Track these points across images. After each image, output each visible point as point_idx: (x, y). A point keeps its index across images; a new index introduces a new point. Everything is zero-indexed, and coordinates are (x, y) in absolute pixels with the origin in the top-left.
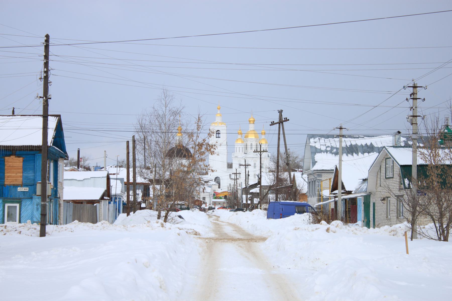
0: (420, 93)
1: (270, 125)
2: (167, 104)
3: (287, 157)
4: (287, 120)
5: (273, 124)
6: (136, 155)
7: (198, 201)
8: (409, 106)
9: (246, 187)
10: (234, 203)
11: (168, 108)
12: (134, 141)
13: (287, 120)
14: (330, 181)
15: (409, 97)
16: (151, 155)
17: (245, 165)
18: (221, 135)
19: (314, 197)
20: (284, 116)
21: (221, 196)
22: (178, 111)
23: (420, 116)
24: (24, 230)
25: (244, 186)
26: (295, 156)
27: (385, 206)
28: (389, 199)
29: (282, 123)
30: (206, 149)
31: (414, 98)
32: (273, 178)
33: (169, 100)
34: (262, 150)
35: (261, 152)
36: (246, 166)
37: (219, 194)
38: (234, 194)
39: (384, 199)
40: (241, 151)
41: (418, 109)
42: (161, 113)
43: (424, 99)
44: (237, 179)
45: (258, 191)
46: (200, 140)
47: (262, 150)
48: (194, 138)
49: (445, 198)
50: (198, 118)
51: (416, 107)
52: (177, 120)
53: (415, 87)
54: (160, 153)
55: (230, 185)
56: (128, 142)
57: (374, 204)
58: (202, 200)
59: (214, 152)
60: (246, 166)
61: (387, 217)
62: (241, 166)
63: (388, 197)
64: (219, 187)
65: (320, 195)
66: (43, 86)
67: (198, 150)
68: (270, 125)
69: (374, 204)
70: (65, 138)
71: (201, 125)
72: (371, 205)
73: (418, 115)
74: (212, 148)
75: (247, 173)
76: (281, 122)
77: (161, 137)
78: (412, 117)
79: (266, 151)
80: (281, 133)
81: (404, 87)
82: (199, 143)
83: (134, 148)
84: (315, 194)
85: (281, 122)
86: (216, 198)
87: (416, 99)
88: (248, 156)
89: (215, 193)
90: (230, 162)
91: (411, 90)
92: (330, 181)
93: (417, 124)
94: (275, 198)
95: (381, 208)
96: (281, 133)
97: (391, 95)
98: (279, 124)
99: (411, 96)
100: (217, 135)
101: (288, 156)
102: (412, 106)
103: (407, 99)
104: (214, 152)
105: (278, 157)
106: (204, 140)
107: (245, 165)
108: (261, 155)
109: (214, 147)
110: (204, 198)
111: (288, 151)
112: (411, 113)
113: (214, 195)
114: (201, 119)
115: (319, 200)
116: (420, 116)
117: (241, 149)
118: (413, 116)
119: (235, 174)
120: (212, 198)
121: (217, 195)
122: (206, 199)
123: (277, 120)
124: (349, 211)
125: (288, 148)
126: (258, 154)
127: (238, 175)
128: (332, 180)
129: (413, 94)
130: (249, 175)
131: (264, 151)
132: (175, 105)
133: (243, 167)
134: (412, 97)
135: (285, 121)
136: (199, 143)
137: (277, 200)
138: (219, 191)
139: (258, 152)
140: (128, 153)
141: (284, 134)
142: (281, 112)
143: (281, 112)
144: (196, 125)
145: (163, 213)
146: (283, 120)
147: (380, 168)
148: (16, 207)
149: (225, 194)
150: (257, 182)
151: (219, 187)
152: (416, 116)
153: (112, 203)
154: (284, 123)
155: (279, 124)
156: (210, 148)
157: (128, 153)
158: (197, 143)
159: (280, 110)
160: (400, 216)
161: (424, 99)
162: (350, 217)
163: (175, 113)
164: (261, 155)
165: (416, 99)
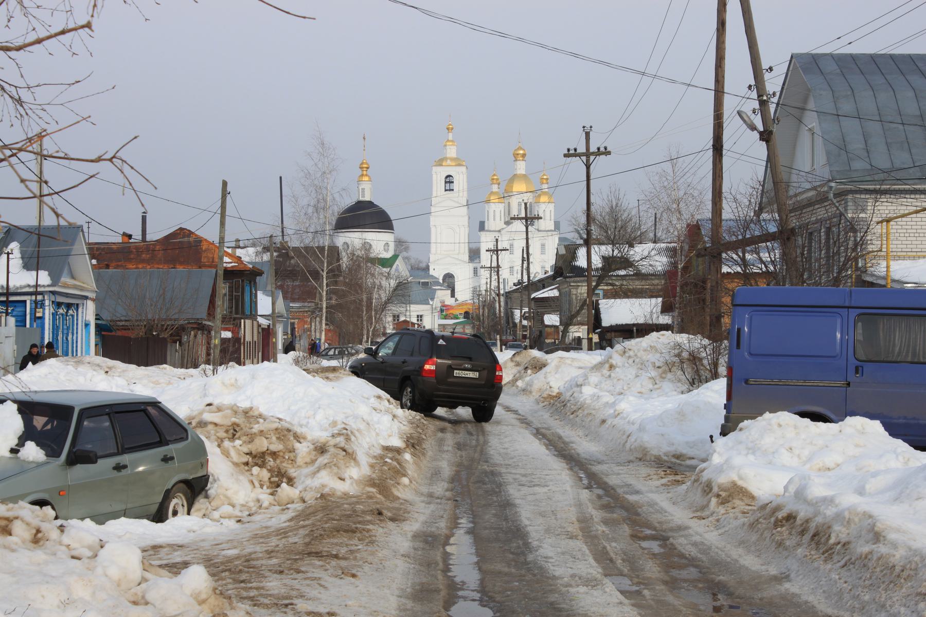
1: (565, 156)
18: (455, 186)
21: (457, 312)
24: (617, 359)
34: (593, 149)
45: (555, 293)
47: (593, 149)
58: (414, 320)
64: (453, 295)
68: (565, 156)
76: (588, 156)
77: (525, 475)
86: (446, 317)
90: (474, 246)
100: (448, 185)
108: (588, 167)
110: (420, 317)
113: (442, 311)
122: (424, 319)
125: (765, 66)
126: (578, 165)
131: (599, 153)
133: (519, 226)
138: (450, 301)
139: (580, 155)
148: (25, 302)
149: (465, 309)
151: (453, 295)
164: (588, 167)
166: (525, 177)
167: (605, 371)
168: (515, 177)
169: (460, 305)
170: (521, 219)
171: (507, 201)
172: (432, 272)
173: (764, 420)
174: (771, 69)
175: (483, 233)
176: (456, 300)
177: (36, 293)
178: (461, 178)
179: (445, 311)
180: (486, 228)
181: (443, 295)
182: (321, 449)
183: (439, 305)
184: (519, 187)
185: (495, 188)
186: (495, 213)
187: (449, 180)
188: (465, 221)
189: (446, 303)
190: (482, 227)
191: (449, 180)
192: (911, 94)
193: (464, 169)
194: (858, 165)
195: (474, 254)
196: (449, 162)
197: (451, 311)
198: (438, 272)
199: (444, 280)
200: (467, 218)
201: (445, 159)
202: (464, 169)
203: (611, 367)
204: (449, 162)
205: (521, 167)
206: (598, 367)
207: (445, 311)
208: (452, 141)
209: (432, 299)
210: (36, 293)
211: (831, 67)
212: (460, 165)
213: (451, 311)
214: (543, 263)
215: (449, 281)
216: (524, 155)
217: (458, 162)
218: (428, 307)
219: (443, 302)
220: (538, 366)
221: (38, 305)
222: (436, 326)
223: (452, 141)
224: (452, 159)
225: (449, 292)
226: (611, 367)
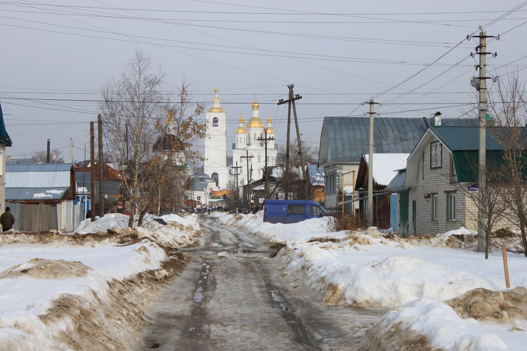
0: (490, 46)
1: (278, 104)
2: (142, 69)
3: (299, 144)
4: (299, 97)
5: (281, 102)
6: (104, 140)
7: (191, 200)
8: (474, 64)
9: (248, 184)
10: (236, 202)
11: (142, 76)
12: (100, 122)
13: (299, 97)
14: (354, 175)
15: (474, 51)
16: (119, 139)
17: (247, 157)
18: (219, 123)
19: (332, 195)
20: (295, 92)
21: (219, 195)
22: (156, 81)
23: (489, 78)
25: (246, 183)
26: (307, 146)
27: (430, 205)
28: (435, 196)
29: (293, 101)
30: (194, 129)
31: (482, 52)
32: (282, 172)
33: (144, 65)
34: (268, 138)
35: (266, 140)
36: (248, 158)
37: (216, 192)
38: (235, 192)
39: (428, 196)
40: (243, 142)
41: (487, 68)
42: (133, 82)
43: (496, 54)
44: (237, 174)
45: (263, 188)
46: (185, 118)
47: (268, 138)
48: (178, 116)
49: (493, 196)
50: (182, 90)
51: (485, 65)
52: (155, 92)
53: (482, 37)
54: (132, 136)
55: (230, 182)
56: (92, 123)
57: (414, 203)
58: (196, 200)
59: (204, 134)
60: (248, 158)
61: (433, 220)
62: (243, 158)
63: (433, 194)
64: (217, 185)
65: (340, 193)
66: (293, 224)
67: (182, 132)
68: (278, 104)
69: (414, 203)
70: (4, 116)
71: (186, 98)
72: (411, 203)
73: (487, 76)
74: (201, 129)
75: (250, 168)
76: (292, 100)
78: (478, 80)
79: (273, 139)
80: (292, 119)
81: (468, 37)
82: (183, 122)
83: (100, 130)
84: (335, 191)
85: (292, 100)
86: (213, 198)
87: (485, 54)
88: (250, 148)
89: (212, 191)
90: (230, 156)
91: (477, 41)
92: (354, 175)
93: (486, 89)
94: (284, 196)
95: (424, 208)
96: (292, 119)
97: (450, 48)
98: (290, 102)
99: (477, 50)
101: (300, 143)
102: (478, 64)
103: (472, 54)
104: (204, 134)
105: (288, 147)
106: (191, 118)
107: (247, 157)
109: (204, 128)
110: (199, 198)
111: (301, 137)
112: (477, 74)
113: (211, 194)
114: (187, 90)
115: (340, 199)
116: (489, 78)
117: (243, 140)
118: (480, 78)
119: (235, 168)
120: (208, 197)
121: (214, 194)
123: (286, 98)
124: (378, 212)
125: (300, 133)
127: (239, 169)
128: (356, 173)
129: (480, 46)
130: (252, 170)
131: (270, 139)
132: (152, 72)
133: (245, 160)
134: (478, 52)
135: (296, 99)
136: (183, 122)
137: (286, 198)
138: (216, 189)
140: (92, 138)
141: (296, 119)
142: (291, 87)
143: (291, 87)
144: (180, 98)
145: (136, 217)
146: (295, 97)
147: (423, 156)
150: (261, 177)
151: (217, 185)
152: (485, 78)
153: (79, 203)
154: (295, 101)
155: (290, 102)
156: (200, 131)
157: (92, 138)
158: (181, 123)
159: (290, 84)
160: (451, 219)
161: (496, 54)
162: (379, 220)
163: (153, 83)
165: (485, 54)
166: (258, 119)
167: (254, 219)
168: (252, 120)
169: (221, 191)
170: (245, 157)
171: (248, 133)
172: (205, 172)
173: (491, 283)
174: (302, 134)
175: (234, 150)
176: (219, 188)
177: (83, 194)
178: (222, 117)
179: (213, 194)
180: (236, 147)
181: (212, 185)
182: (188, 228)
183: (209, 191)
184: (255, 124)
185: (241, 125)
186: (241, 138)
187: (215, 120)
188: (224, 143)
189: (213, 190)
190: (234, 147)
191: (215, 120)
192: (359, 132)
193: (224, 114)
194: (340, 156)
195: (229, 161)
196: (215, 110)
197: (216, 194)
198: (208, 172)
199: (212, 176)
200: (225, 142)
201: (214, 108)
202: (224, 114)
203: (256, 217)
204: (215, 110)
205: (256, 113)
206: (253, 217)
207: (213, 194)
208: (217, 98)
209: (206, 188)
210: (83, 194)
211: (336, 122)
212: (222, 112)
213: (216, 194)
214: (257, 176)
215: (215, 177)
216: (258, 107)
217: (221, 110)
218: (203, 192)
219: (211, 189)
220: (240, 218)
221: (84, 198)
222: (208, 203)
223: (217, 98)
224: (217, 109)
225: (215, 183)
226: (256, 217)
